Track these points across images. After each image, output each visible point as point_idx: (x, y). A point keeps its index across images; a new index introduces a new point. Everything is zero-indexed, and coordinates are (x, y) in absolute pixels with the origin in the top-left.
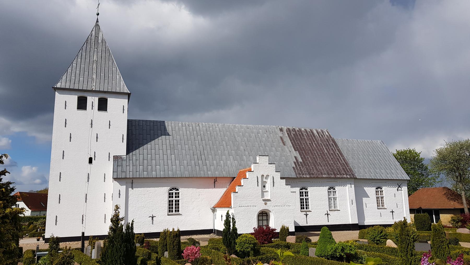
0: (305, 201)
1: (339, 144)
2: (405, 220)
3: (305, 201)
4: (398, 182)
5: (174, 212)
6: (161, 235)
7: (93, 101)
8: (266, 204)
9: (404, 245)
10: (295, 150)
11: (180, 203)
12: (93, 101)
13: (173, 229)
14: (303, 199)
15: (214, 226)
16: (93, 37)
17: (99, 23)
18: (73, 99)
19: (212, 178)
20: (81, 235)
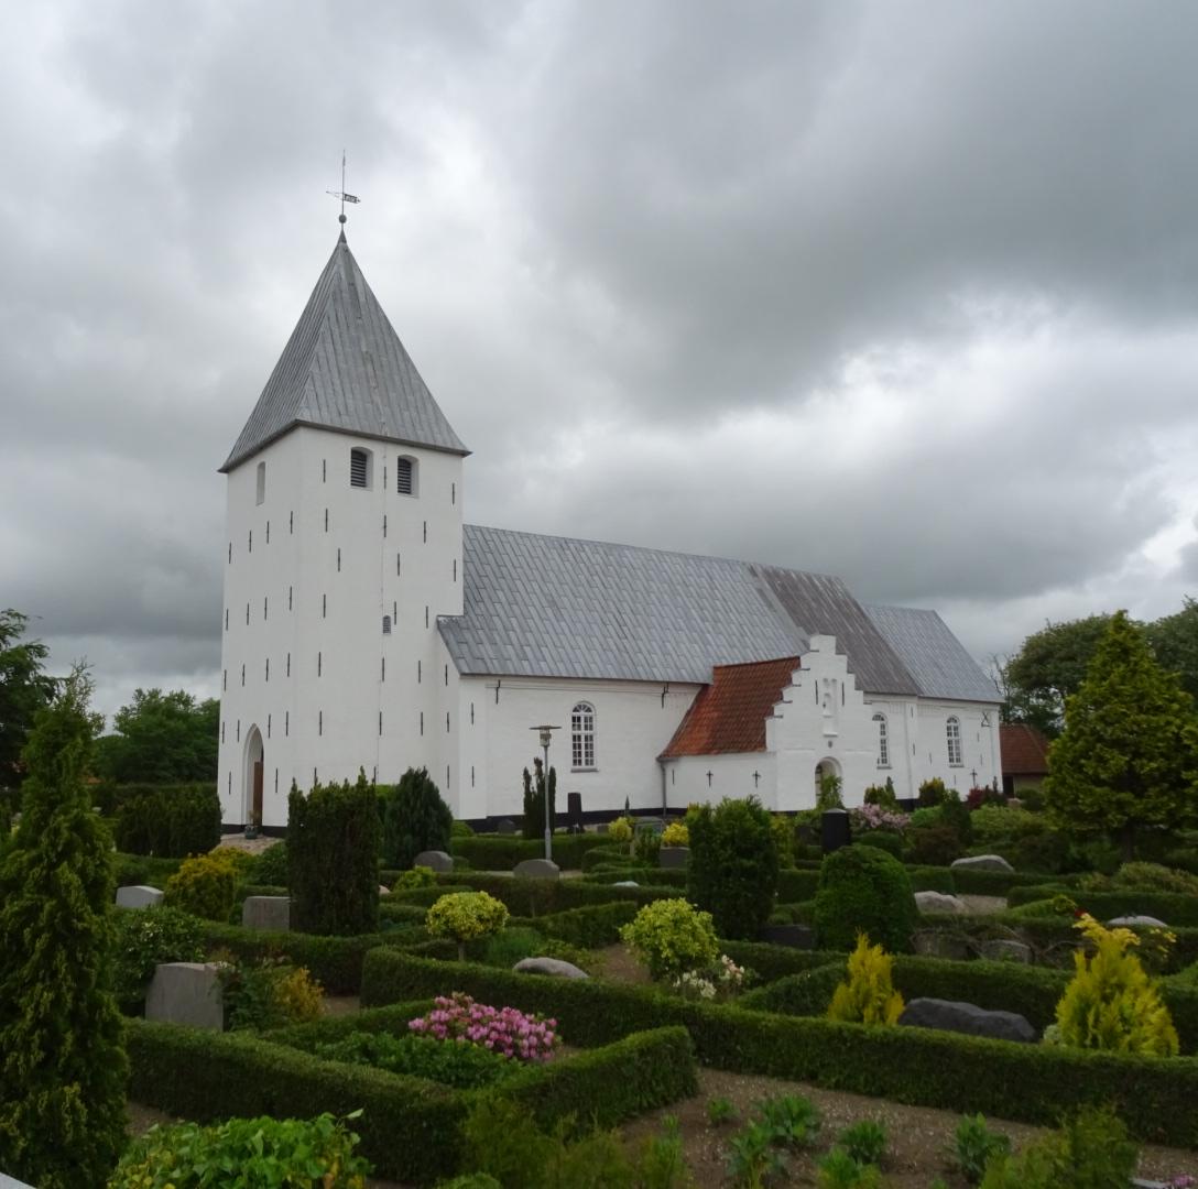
0: (583, 742)
1: (873, 617)
2: (987, 787)
3: (583, 742)
4: (985, 707)
5: (583, 766)
6: (690, 814)
7: (384, 461)
8: (830, 744)
9: (575, 1074)
10: (797, 625)
11: (597, 742)
12: (384, 461)
13: (828, 782)
14: (579, 737)
15: (665, 803)
16: (345, 285)
17: (350, 244)
18: (339, 452)
19: (663, 682)
20: (623, 807)
